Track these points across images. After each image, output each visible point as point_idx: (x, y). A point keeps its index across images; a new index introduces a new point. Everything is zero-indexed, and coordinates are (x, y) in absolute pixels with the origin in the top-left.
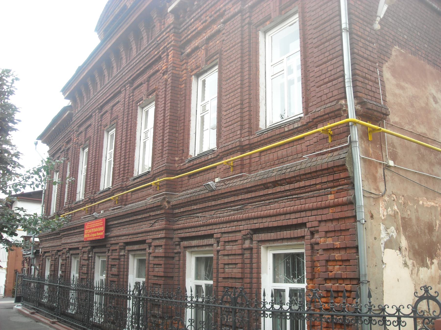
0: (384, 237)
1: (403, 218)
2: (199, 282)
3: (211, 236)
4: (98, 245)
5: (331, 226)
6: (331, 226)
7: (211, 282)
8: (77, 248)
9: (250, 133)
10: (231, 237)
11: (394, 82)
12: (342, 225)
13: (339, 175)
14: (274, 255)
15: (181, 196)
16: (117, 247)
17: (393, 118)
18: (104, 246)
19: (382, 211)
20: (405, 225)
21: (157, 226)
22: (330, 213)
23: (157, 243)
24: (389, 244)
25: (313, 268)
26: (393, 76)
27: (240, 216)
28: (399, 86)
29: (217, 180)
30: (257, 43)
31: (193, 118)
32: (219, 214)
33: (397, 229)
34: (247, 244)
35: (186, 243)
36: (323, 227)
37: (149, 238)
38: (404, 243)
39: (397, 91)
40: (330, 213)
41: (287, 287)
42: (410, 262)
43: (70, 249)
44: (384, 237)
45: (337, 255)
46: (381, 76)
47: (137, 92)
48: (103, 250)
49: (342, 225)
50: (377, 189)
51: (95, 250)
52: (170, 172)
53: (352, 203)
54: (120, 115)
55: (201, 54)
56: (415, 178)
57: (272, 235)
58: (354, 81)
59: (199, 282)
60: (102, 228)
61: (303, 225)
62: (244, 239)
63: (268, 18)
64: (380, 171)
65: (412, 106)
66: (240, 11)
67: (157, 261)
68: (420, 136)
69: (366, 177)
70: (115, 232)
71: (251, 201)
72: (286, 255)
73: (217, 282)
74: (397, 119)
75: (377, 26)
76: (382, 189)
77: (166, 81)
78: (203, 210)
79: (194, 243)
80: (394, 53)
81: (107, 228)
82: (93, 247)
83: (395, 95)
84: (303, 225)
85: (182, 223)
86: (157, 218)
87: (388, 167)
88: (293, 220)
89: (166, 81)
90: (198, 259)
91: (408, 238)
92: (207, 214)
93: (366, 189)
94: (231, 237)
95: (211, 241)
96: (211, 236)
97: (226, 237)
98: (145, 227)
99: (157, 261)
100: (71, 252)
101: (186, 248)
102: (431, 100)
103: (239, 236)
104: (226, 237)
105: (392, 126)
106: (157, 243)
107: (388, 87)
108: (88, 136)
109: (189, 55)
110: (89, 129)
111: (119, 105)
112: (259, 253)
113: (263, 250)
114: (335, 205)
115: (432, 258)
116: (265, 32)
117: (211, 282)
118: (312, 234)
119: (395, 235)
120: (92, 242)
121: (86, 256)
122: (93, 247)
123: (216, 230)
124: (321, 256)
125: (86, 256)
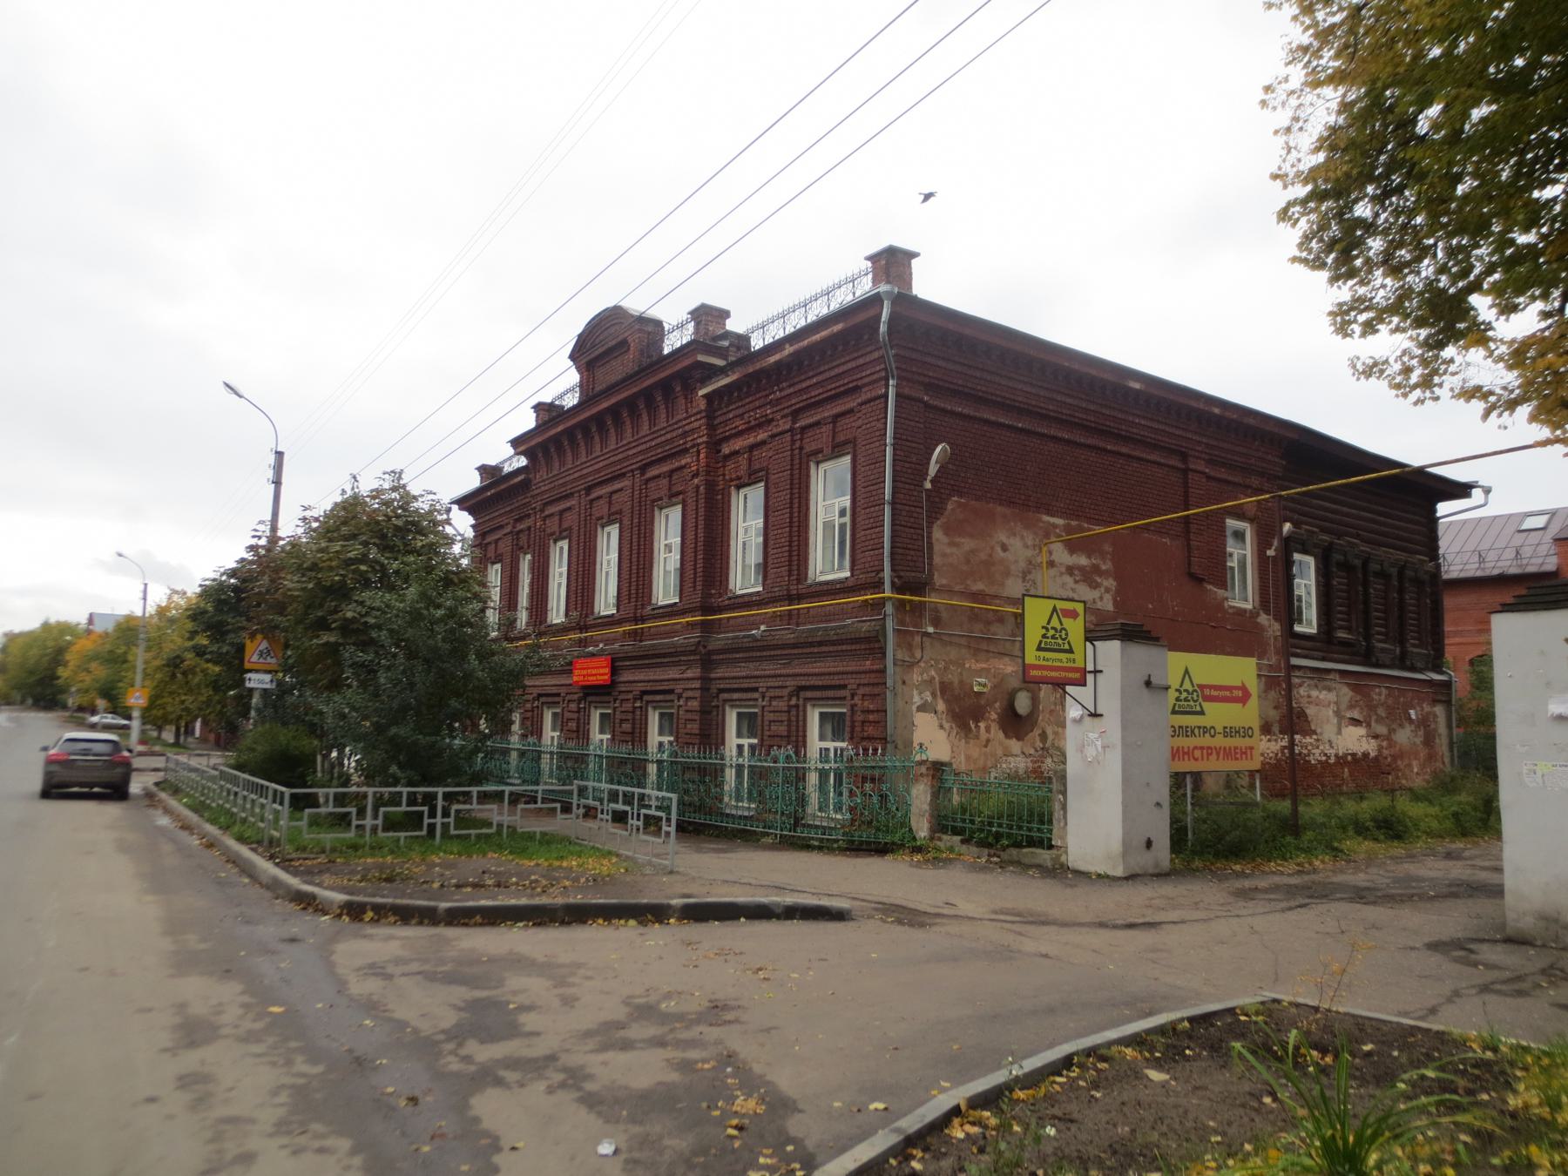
0: (917, 700)
1: (942, 683)
2: (741, 741)
3: (755, 690)
4: (594, 693)
5: (867, 690)
6: (867, 690)
7: (755, 741)
8: (558, 695)
9: (799, 581)
10: (778, 692)
11: (945, 540)
12: (876, 690)
13: (873, 644)
14: (821, 714)
15: (720, 640)
16: (630, 696)
17: (939, 580)
18: (609, 694)
19: (916, 677)
20: (945, 688)
21: (689, 674)
22: (865, 679)
23: (690, 694)
24: (923, 708)
25: (853, 727)
26: (946, 534)
27: (783, 672)
28: (952, 544)
29: (763, 628)
30: (808, 476)
31: (733, 543)
32: (765, 665)
33: (934, 695)
34: (794, 701)
35: (726, 696)
36: (861, 691)
37: (679, 688)
38: (941, 706)
39: (948, 551)
40: (865, 679)
41: (831, 745)
42: (947, 726)
43: (540, 695)
44: (917, 700)
45: (871, 717)
46: (929, 537)
47: (652, 485)
48: (606, 698)
49: (876, 690)
50: (913, 656)
51: (590, 699)
52: (707, 609)
53: (883, 671)
54: (627, 508)
55: (743, 461)
56: (963, 641)
57: (818, 694)
58: (892, 554)
59: (741, 741)
60: (606, 670)
61: (844, 687)
62: (790, 696)
63: (820, 451)
64: (918, 639)
65: (968, 562)
66: (791, 430)
67: (689, 716)
68: (976, 597)
69: (898, 645)
70: (626, 676)
71: (798, 656)
72: (833, 714)
73: (762, 740)
74: (944, 582)
75: (928, 485)
76: (918, 655)
77: (698, 487)
78: (747, 660)
79: (736, 696)
80: (950, 507)
81: (614, 671)
82: (586, 695)
83: (944, 555)
84: (844, 687)
85: (719, 673)
86: (689, 664)
87: (928, 635)
88: (836, 681)
89: (698, 487)
90: (739, 714)
91: (947, 702)
92: (751, 665)
93: (899, 656)
94: (778, 692)
95: (756, 695)
96: (755, 690)
97: (772, 693)
98: (673, 673)
99: (689, 716)
100: (543, 699)
101: (725, 701)
102: (999, 549)
103: (785, 692)
104: (772, 693)
105: (939, 591)
106: (690, 694)
107: (936, 548)
108: (565, 526)
109: (727, 457)
110: (567, 514)
111: (622, 494)
112: (805, 711)
113: (809, 708)
114: (871, 672)
115: (977, 721)
116: (818, 463)
117: (755, 741)
118: (853, 696)
119: (929, 699)
120: (584, 688)
121: (573, 706)
122: (586, 695)
123: (762, 684)
124: (859, 717)
125: (573, 706)
